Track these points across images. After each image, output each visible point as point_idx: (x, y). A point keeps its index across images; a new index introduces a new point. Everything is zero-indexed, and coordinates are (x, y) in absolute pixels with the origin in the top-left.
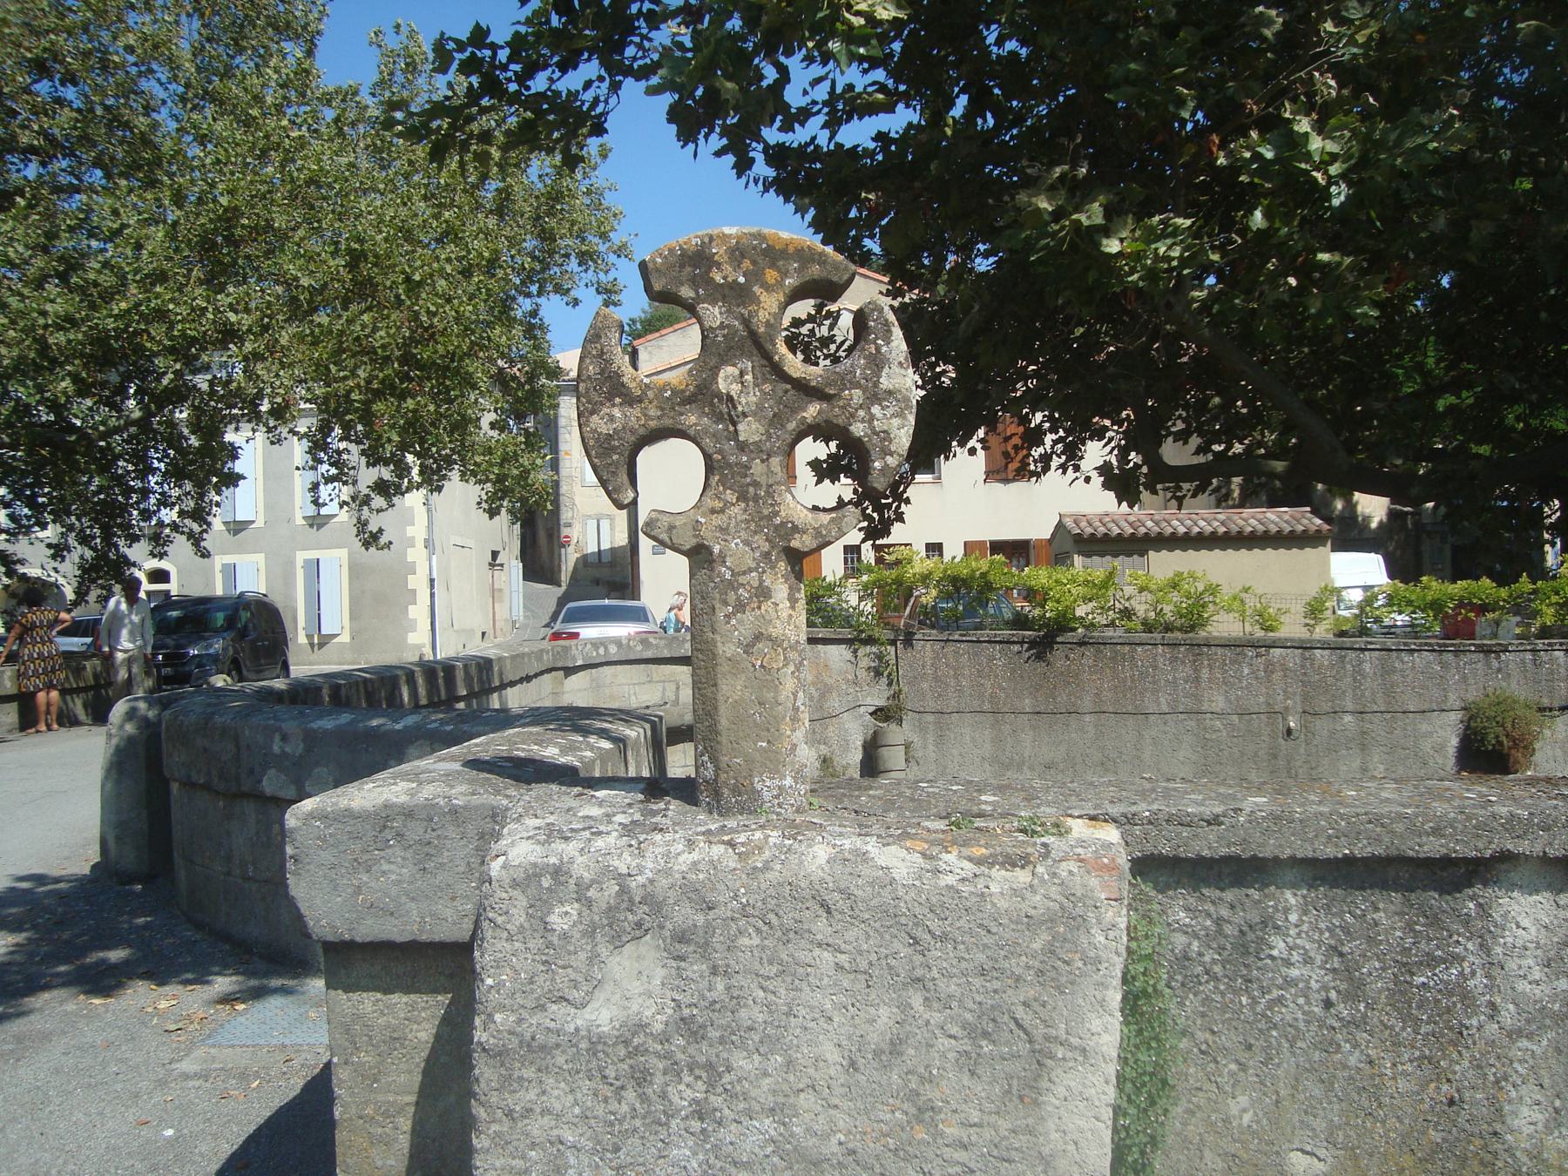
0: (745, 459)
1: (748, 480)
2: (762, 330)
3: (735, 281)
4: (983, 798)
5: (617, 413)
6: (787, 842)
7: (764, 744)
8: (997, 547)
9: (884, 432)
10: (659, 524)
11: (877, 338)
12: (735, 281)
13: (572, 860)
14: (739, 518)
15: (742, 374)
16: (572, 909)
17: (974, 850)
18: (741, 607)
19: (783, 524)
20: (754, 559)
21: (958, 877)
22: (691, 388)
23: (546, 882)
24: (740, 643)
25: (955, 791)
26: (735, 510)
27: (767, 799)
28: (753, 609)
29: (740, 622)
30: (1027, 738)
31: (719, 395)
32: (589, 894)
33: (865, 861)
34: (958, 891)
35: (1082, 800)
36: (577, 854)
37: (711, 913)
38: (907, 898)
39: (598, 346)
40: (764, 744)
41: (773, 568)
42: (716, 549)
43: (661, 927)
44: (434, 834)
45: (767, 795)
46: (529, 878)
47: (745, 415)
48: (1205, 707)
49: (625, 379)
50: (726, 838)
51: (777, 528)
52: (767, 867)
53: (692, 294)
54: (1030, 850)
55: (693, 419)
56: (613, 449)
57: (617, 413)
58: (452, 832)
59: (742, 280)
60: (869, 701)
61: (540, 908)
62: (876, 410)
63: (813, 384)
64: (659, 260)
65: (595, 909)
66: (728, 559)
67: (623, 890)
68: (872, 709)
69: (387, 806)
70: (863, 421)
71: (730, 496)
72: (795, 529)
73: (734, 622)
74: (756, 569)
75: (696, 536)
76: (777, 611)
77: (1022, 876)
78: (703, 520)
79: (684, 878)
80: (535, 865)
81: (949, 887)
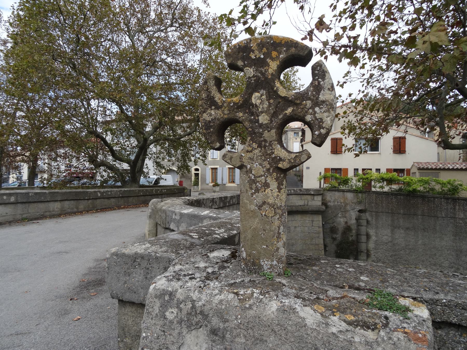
0: (261, 130)
1: (262, 139)
2: (270, 77)
3: (259, 57)
4: (362, 278)
5: (213, 112)
6: (261, 297)
7: (265, 247)
8: (395, 170)
9: (320, 119)
10: (227, 156)
11: (319, 78)
12: (259, 57)
13: (176, 291)
14: (258, 154)
15: (262, 95)
16: (175, 311)
17: (347, 316)
18: (257, 190)
19: (276, 157)
20: (263, 171)
21: (338, 330)
22: (241, 102)
23: (167, 298)
24: (257, 205)
25: (350, 272)
26: (257, 151)
27: (265, 269)
28: (262, 192)
29: (257, 196)
30: (401, 221)
31: (252, 104)
32: (181, 306)
33: (294, 313)
34: (337, 337)
35: (410, 286)
36: (179, 288)
37: (227, 323)
38: (312, 335)
39: (206, 86)
40: (265, 247)
41: (271, 175)
42: (249, 167)
43: (206, 326)
44: (150, 266)
45: (265, 268)
46: (162, 294)
47: (262, 112)
48: (457, 216)
49: (216, 99)
50: (235, 291)
51: (273, 159)
52: (250, 307)
53: (242, 64)
54: (377, 321)
55: (241, 114)
56: (211, 127)
57: (213, 112)
58: (155, 265)
59: (262, 56)
60: (357, 208)
61: (164, 307)
62: (317, 109)
63: (290, 99)
64: (230, 51)
65: (183, 313)
66: (253, 171)
67: (193, 307)
68: (358, 210)
69: (136, 253)
70: (311, 114)
71: (255, 145)
72: (281, 159)
73: (254, 196)
74: (264, 175)
75: (241, 161)
76: (272, 193)
77: (371, 335)
78: (243, 155)
79: (216, 306)
80: (164, 290)
81: (333, 334)
